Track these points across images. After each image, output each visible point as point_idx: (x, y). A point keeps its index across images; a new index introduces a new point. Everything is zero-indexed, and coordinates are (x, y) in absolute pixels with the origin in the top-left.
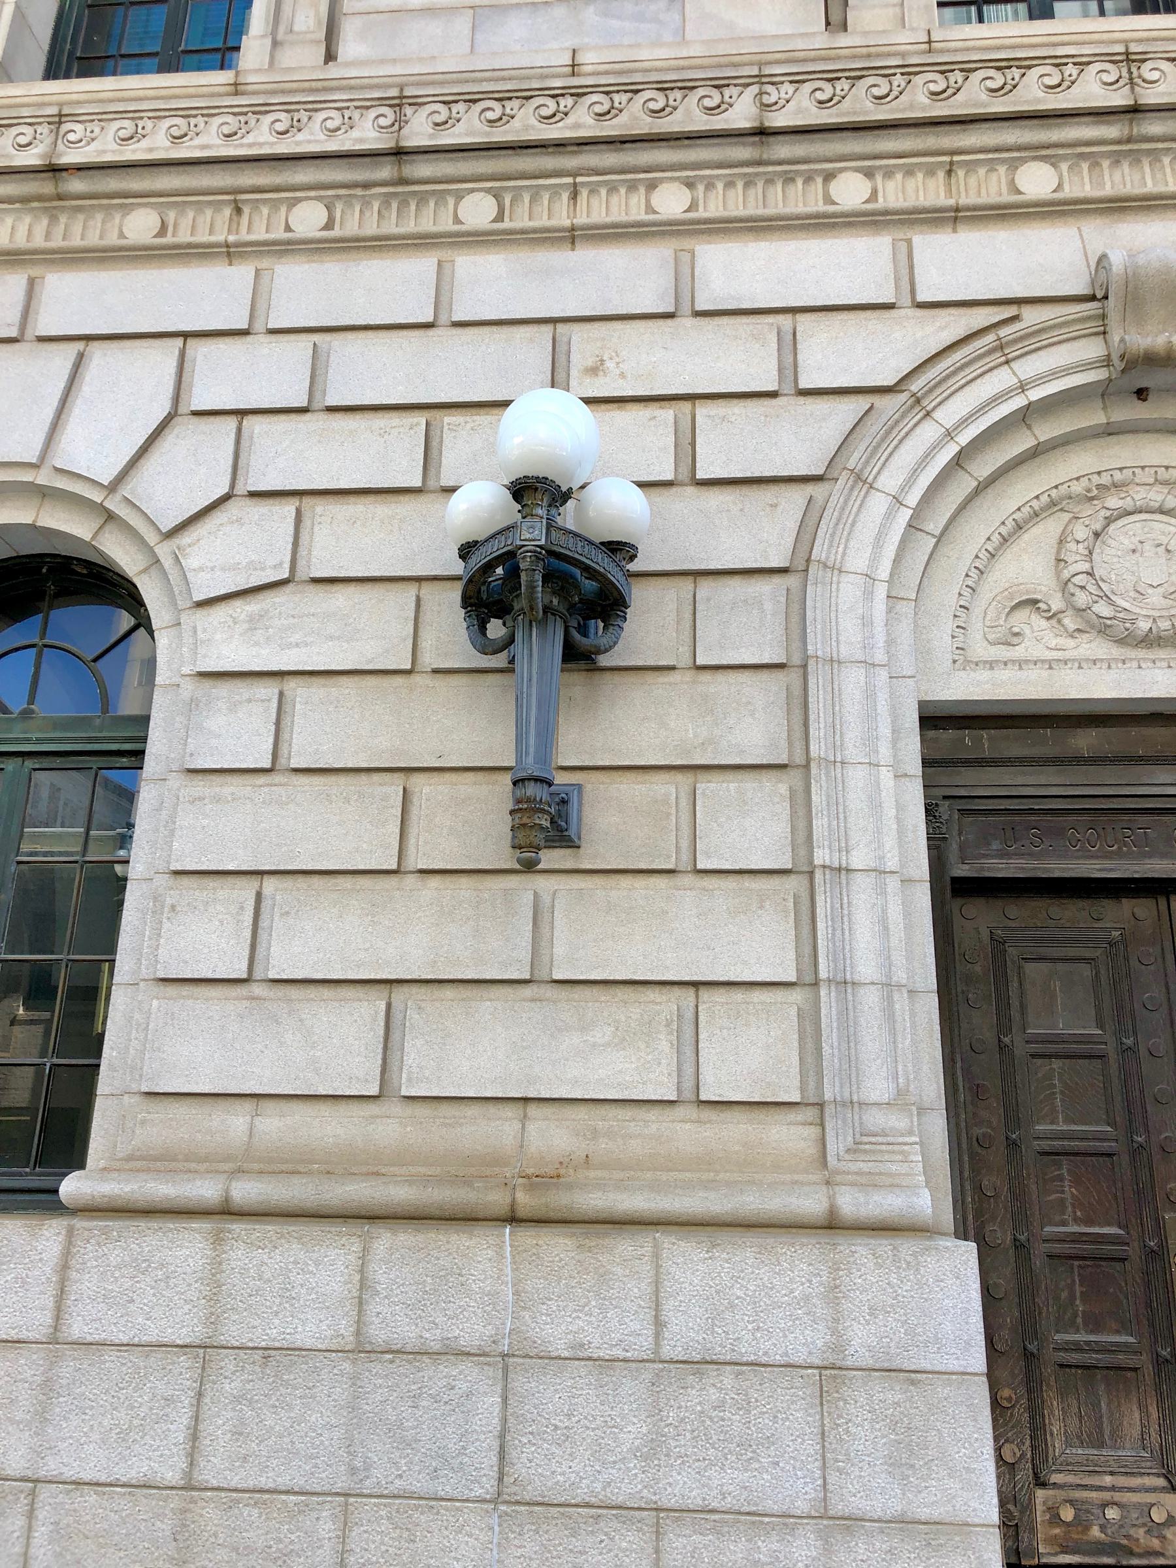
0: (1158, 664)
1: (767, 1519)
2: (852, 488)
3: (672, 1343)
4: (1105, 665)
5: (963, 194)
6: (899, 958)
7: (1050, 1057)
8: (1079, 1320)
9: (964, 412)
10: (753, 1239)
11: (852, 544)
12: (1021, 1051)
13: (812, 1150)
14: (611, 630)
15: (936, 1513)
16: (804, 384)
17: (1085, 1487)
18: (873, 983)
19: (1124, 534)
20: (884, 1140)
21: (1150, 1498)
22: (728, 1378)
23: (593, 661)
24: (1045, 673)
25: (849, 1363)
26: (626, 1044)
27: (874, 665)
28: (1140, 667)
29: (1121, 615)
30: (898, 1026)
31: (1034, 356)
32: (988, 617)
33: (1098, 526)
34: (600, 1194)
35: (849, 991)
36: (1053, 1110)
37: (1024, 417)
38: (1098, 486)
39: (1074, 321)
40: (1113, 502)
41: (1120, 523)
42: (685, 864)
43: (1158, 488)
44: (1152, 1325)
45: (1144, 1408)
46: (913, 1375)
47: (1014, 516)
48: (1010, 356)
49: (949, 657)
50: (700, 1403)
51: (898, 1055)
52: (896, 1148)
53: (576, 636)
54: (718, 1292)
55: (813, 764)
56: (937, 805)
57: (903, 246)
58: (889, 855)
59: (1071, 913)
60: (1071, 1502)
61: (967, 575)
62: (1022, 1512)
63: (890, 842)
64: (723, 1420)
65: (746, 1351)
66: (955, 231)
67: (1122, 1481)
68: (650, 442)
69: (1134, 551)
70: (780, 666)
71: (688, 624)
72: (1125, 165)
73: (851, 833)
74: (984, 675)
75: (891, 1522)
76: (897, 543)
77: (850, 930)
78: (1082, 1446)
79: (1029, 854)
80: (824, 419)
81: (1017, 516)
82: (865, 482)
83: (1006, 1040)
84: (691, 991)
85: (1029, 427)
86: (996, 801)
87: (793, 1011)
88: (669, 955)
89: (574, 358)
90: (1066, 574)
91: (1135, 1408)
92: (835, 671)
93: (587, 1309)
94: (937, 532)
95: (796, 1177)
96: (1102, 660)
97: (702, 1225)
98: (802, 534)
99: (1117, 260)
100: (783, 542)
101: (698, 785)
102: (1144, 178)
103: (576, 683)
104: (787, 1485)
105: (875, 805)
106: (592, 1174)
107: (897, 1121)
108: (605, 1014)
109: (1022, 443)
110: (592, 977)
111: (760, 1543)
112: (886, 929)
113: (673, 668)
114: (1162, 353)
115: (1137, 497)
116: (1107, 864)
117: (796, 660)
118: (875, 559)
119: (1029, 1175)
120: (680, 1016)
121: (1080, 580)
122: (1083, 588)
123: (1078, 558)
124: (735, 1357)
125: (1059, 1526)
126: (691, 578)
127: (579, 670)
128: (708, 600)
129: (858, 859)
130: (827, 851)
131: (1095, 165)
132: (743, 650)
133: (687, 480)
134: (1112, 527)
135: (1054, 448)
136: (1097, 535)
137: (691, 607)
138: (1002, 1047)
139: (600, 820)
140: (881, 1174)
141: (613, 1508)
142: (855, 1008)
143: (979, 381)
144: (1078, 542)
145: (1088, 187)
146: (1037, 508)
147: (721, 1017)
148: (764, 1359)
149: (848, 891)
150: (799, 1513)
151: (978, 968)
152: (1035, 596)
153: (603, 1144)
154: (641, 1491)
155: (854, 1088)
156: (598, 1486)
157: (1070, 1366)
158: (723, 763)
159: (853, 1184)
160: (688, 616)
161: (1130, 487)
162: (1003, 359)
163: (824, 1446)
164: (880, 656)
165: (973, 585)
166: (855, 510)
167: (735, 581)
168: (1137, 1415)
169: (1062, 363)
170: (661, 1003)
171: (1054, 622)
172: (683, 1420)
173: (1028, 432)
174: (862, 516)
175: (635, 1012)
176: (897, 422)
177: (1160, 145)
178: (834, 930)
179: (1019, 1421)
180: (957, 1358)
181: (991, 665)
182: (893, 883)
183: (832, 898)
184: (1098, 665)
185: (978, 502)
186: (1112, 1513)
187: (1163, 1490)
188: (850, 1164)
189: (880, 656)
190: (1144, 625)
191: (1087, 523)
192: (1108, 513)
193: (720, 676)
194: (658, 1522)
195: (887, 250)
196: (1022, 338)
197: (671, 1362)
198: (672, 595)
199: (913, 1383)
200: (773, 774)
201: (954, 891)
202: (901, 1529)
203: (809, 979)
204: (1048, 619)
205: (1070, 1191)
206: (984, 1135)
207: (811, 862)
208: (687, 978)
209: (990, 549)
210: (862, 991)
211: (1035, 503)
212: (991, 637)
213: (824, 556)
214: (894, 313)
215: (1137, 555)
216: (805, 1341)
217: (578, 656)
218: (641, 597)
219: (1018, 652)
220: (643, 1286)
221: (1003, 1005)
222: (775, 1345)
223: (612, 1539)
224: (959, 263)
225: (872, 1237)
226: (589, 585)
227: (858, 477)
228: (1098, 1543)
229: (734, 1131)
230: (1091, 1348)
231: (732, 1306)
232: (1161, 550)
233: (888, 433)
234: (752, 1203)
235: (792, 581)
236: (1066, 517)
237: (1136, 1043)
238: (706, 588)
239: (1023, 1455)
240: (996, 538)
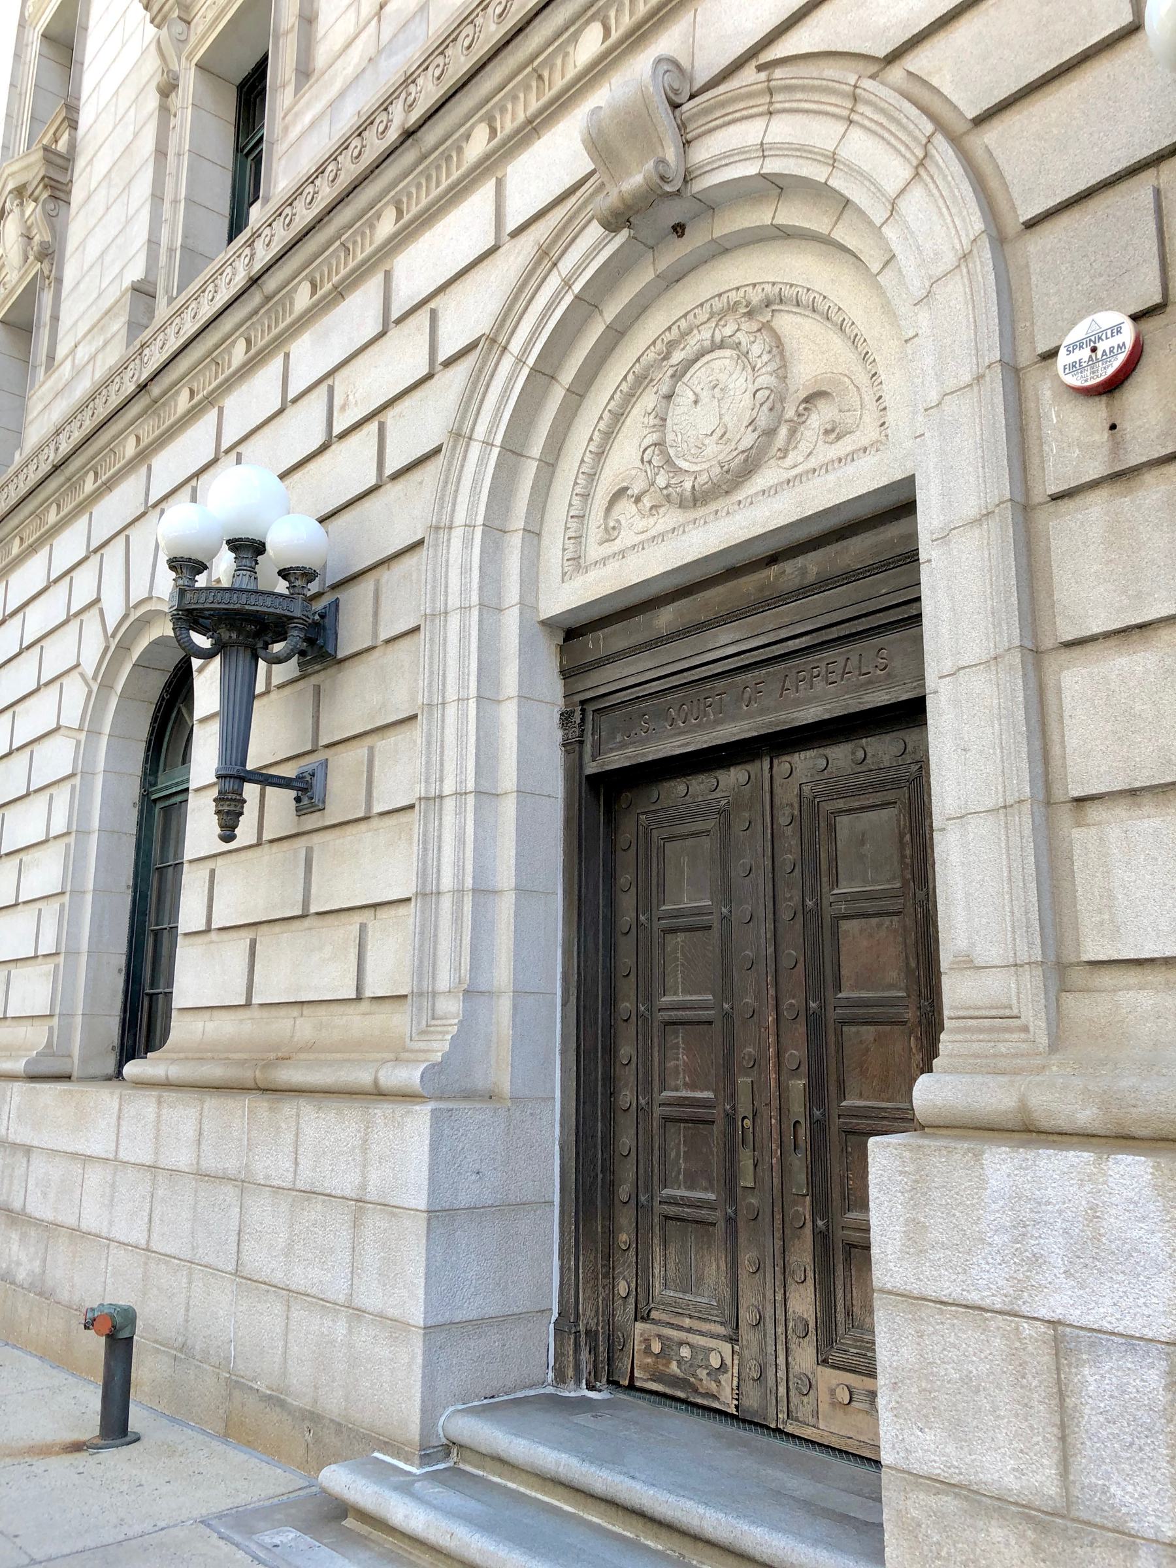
8: (681, 1177)
21: (712, 1343)
40: (677, 357)
45: (717, 1260)
47: (609, 407)
60: (659, 1336)
67: (697, 1325)
109: (595, 331)
186: (685, 1352)
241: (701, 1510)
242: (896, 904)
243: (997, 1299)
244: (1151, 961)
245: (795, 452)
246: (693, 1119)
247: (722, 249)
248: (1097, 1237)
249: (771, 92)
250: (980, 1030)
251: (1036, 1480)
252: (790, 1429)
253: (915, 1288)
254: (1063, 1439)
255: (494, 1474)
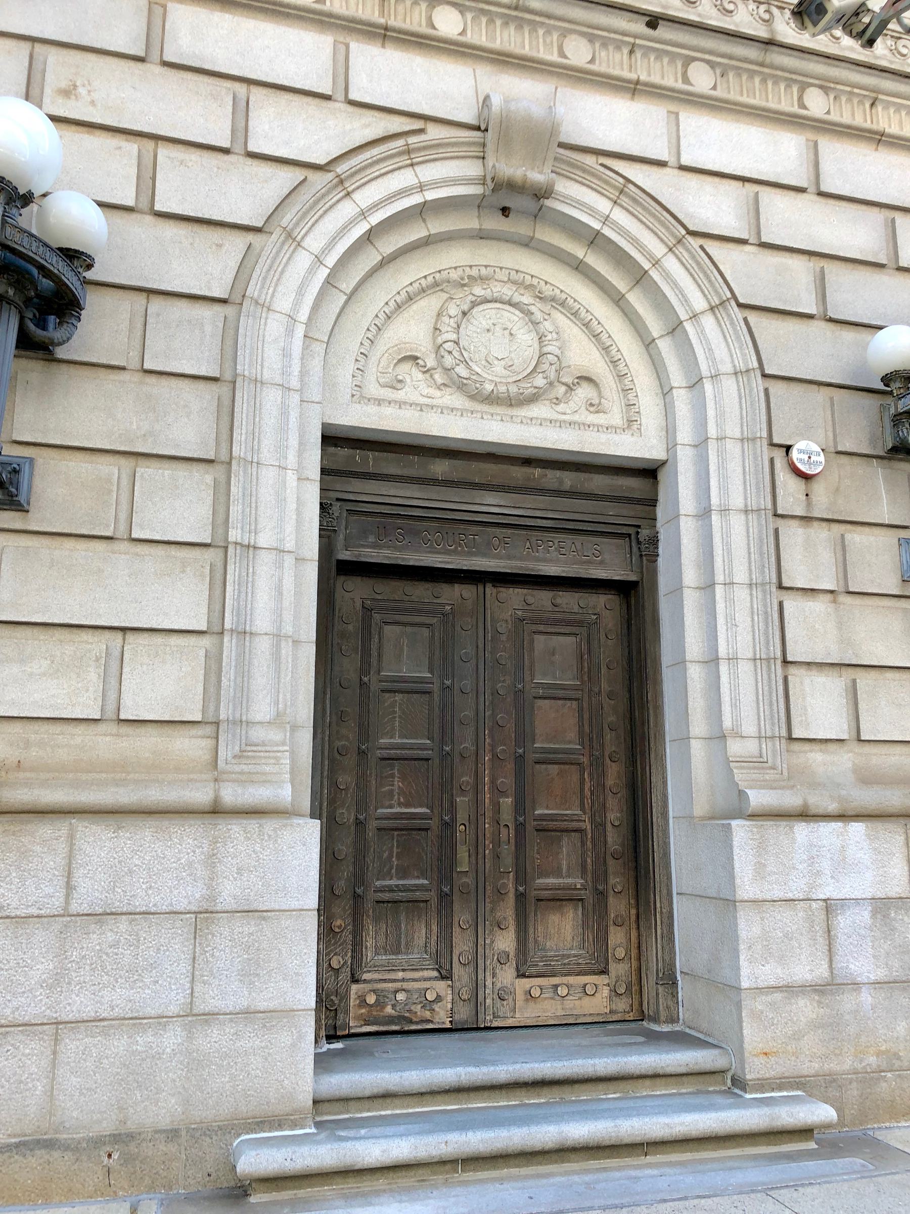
0: (495, 417)
1: (145, 1021)
2: (283, 243)
3: (79, 901)
4: (459, 413)
5: (392, 17)
6: (288, 617)
7: (395, 692)
8: (393, 871)
9: (377, 197)
10: (152, 822)
11: (280, 288)
12: (375, 687)
13: (207, 757)
14: (65, 325)
15: (271, 1005)
16: (252, 148)
17: (385, 981)
18: (266, 634)
19: (484, 316)
20: (263, 749)
21: (427, 984)
22: (123, 924)
23: (51, 353)
24: (417, 414)
25: (218, 908)
26: (60, 674)
27: (289, 389)
28: (482, 418)
29: (474, 377)
30: (283, 667)
31: (432, 165)
32: (381, 365)
33: (465, 307)
34: (26, 790)
35: (247, 639)
36: (393, 729)
37: (422, 211)
38: (469, 277)
39: (463, 144)
40: (478, 291)
41: (481, 307)
42: (122, 532)
43: (509, 285)
44: (440, 872)
45: (428, 926)
46: (265, 914)
47: (407, 289)
48: (414, 160)
49: (349, 391)
50: (99, 944)
51: (281, 687)
52: (272, 754)
53: (32, 327)
54: (120, 862)
55: (233, 462)
56: (331, 504)
57: (342, 48)
58: (288, 539)
59: (420, 591)
60: (374, 991)
61: (368, 329)
62: (340, 1001)
63: (290, 528)
64: (117, 954)
65: (139, 904)
66: (383, 46)
68: (115, 169)
69: (488, 330)
70: (215, 379)
71: (139, 333)
72: (512, 28)
73: (260, 519)
74: (372, 409)
75: (238, 1013)
76: (315, 294)
77: (252, 593)
78: (385, 954)
79: (394, 547)
80: (266, 181)
81: (410, 289)
82: (294, 240)
83: (366, 679)
84: (119, 635)
85: (424, 221)
86: (383, 507)
87: (202, 653)
88: (103, 605)
89: (50, 77)
90: (439, 340)
91: (423, 926)
92: (258, 389)
93: (8, 879)
94: (348, 291)
95: (191, 776)
96: (458, 409)
97: (112, 812)
98: (240, 273)
99: (496, 101)
100: (224, 277)
101: (138, 469)
102: (524, 42)
103: (32, 370)
104: (164, 996)
105: (281, 501)
106: (21, 775)
107: (275, 735)
108: (43, 649)
109: (416, 233)
110: (33, 620)
111: (138, 1038)
112: (281, 594)
113: (123, 368)
114: (520, 183)
115: (494, 290)
116: (446, 558)
117: (228, 376)
118: (297, 304)
119: (371, 774)
120: (108, 654)
121: (449, 346)
122: (450, 352)
123: (449, 329)
124: (130, 909)
125: (364, 1007)
126: (145, 295)
127: (37, 359)
128: (158, 315)
129: (263, 540)
130: (239, 531)
131: (491, 21)
132: (185, 362)
133: (146, 209)
134: (475, 310)
135: (441, 241)
136: (464, 314)
137: (143, 319)
138: (362, 684)
139: (49, 490)
140: (258, 773)
141: (19, 1026)
142: (250, 651)
143: (390, 175)
144: (450, 317)
145: (484, 38)
146: (424, 285)
147: (142, 656)
148: (153, 910)
149: (253, 564)
150: (171, 1014)
151: (350, 627)
152: (416, 354)
153: (34, 752)
154: (44, 1011)
155: (244, 711)
156: (8, 1011)
157: (383, 902)
158: (160, 453)
159: (234, 781)
160: (139, 326)
161: (491, 281)
162: (409, 162)
163: (194, 967)
164: (295, 383)
165: (372, 338)
166: (284, 260)
167: (183, 304)
168: (424, 931)
169: (451, 175)
170: (92, 643)
171: (428, 375)
172: (84, 957)
173: (423, 225)
174: (290, 267)
175: (69, 649)
176: (323, 196)
177: (538, 19)
178: (239, 592)
179: (345, 941)
180: (298, 900)
181: (379, 402)
182: (289, 560)
183: (240, 567)
184: (455, 413)
185: (381, 273)
187: (436, 978)
188: (235, 766)
189: (295, 383)
190: (489, 387)
191: (458, 303)
192: (474, 299)
193: (164, 381)
194: (57, 1032)
195: (329, 50)
196: (425, 148)
197: (78, 915)
198: (124, 308)
199: (264, 919)
200: (202, 467)
201: (336, 570)
202: (246, 1018)
203: (217, 629)
204: (424, 372)
205: (397, 783)
206: (343, 746)
207: (226, 539)
208: (116, 624)
209: (387, 312)
210: (257, 639)
211: (423, 282)
212: (382, 380)
213: (256, 294)
214: (330, 104)
215: (491, 334)
216: (186, 895)
217: (31, 345)
218: (94, 304)
219: (400, 395)
220: (58, 860)
221: (366, 653)
222: (163, 899)
223: (17, 1048)
224: (386, 74)
225: (245, 819)
226: (46, 284)
227: (289, 235)
228: (390, 1016)
229: (147, 742)
230: (399, 889)
231: (131, 872)
232: (507, 332)
233: (316, 203)
234: (154, 795)
235: (229, 310)
236: (445, 296)
237: (453, 684)
238: (156, 305)
239: (345, 963)
240: (392, 304)
241: (591, 1062)
242: (578, 694)
243: (800, 894)
244: (814, 740)
245: (566, 405)
246: (407, 830)
247: (527, 243)
248: (844, 859)
249: (621, 192)
250: (755, 768)
251: (817, 973)
252: (495, 1024)
253: (760, 896)
254: (830, 951)
255: (361, 1111)
